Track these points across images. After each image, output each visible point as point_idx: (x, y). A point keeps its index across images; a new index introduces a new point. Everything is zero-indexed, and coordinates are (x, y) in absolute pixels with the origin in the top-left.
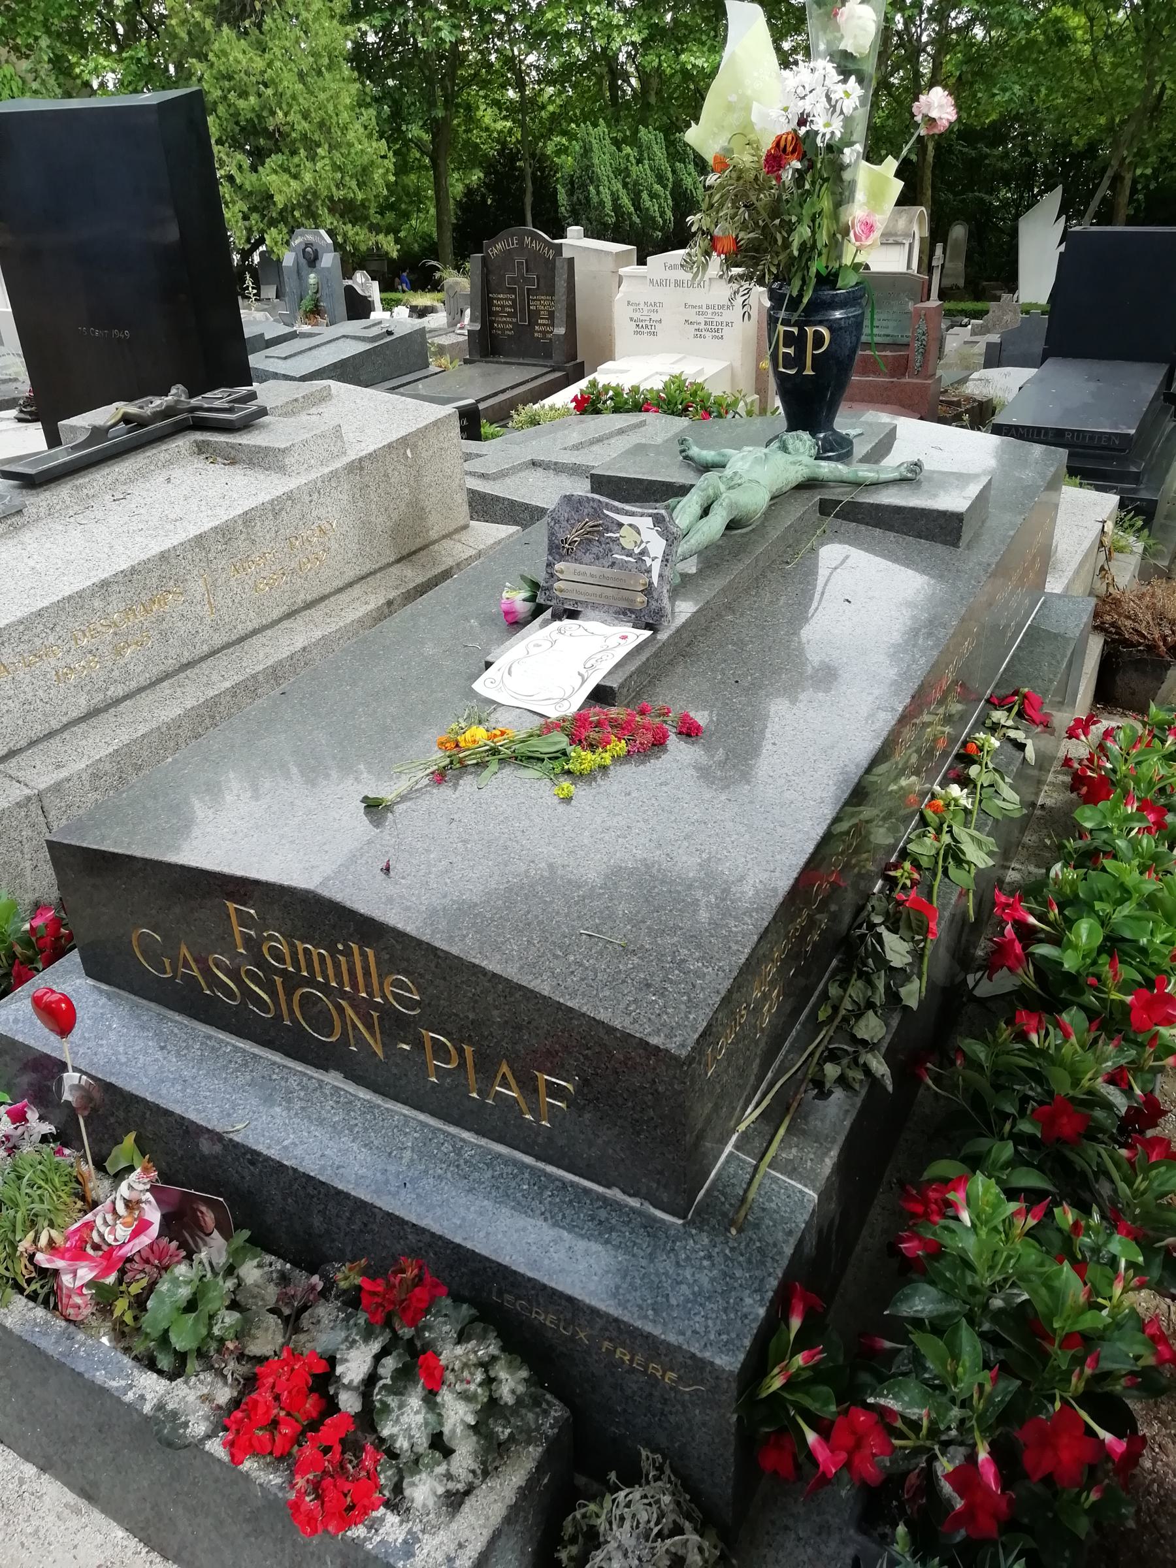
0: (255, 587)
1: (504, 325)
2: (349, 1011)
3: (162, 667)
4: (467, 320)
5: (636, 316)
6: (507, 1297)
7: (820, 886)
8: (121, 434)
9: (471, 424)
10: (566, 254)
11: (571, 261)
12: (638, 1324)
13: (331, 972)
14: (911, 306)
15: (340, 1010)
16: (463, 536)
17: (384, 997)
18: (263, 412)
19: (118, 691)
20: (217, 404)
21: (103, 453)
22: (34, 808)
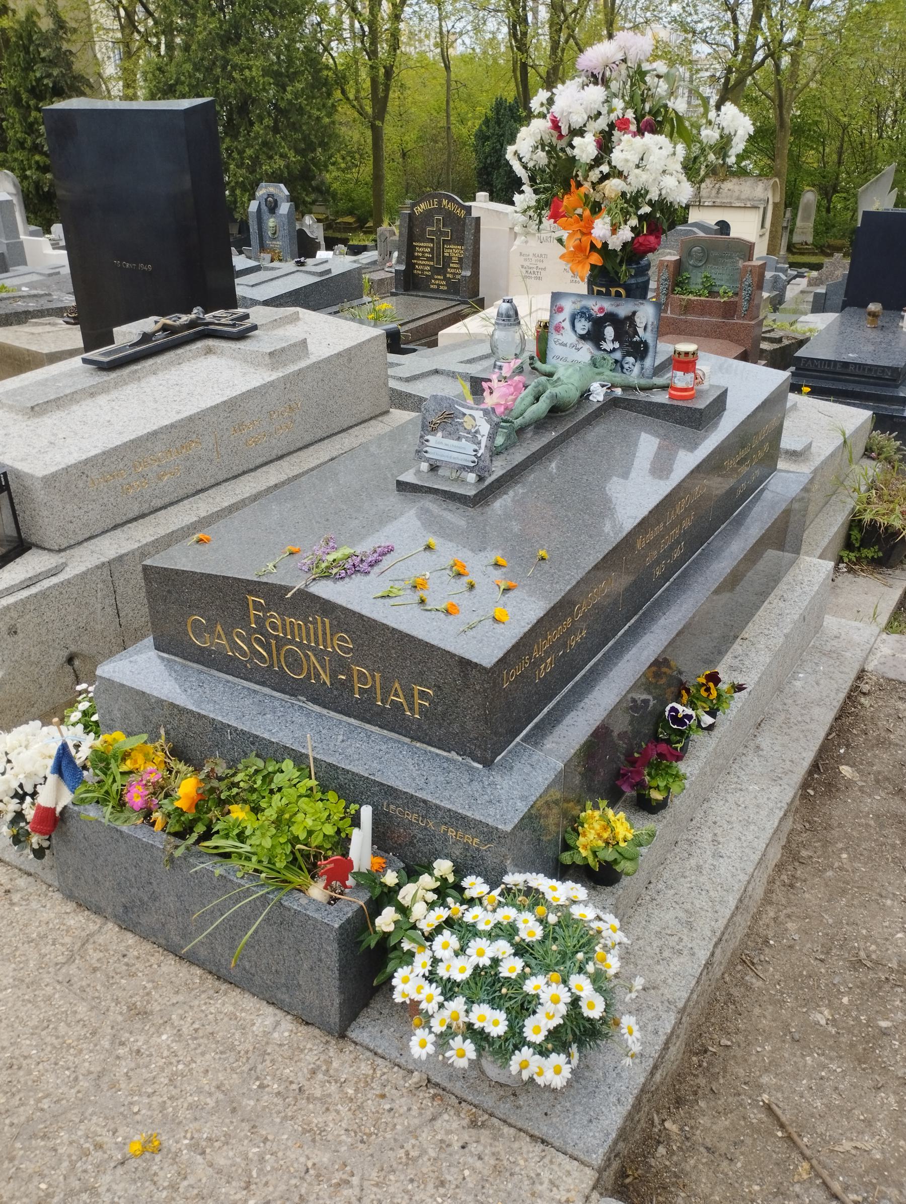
0: (246, 443)
1: (423, 267)
2: (313, 658)
3: (185, 491)
4: (394, 261)
5: (526, 264)
6: (392, 807)
7: (580, 608)
8: (161, 339)
9: (395, 343)
10: (475, 214)
11: (478, 219)
12: (460, 811)
13: (304, 635)
14: (741, 264)
15: (307, 656)
16: (385, 418)
17: (333, 647)
18: (255, 328)
19: (158, 503)
20: (223, 321)
21: (147, 351)
22: (106, 571)
